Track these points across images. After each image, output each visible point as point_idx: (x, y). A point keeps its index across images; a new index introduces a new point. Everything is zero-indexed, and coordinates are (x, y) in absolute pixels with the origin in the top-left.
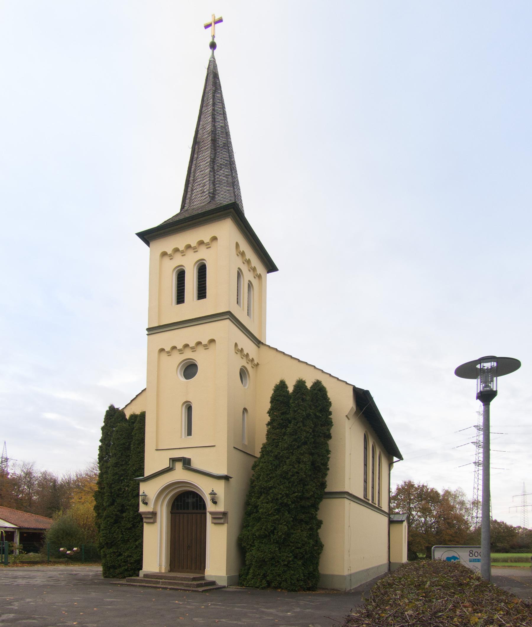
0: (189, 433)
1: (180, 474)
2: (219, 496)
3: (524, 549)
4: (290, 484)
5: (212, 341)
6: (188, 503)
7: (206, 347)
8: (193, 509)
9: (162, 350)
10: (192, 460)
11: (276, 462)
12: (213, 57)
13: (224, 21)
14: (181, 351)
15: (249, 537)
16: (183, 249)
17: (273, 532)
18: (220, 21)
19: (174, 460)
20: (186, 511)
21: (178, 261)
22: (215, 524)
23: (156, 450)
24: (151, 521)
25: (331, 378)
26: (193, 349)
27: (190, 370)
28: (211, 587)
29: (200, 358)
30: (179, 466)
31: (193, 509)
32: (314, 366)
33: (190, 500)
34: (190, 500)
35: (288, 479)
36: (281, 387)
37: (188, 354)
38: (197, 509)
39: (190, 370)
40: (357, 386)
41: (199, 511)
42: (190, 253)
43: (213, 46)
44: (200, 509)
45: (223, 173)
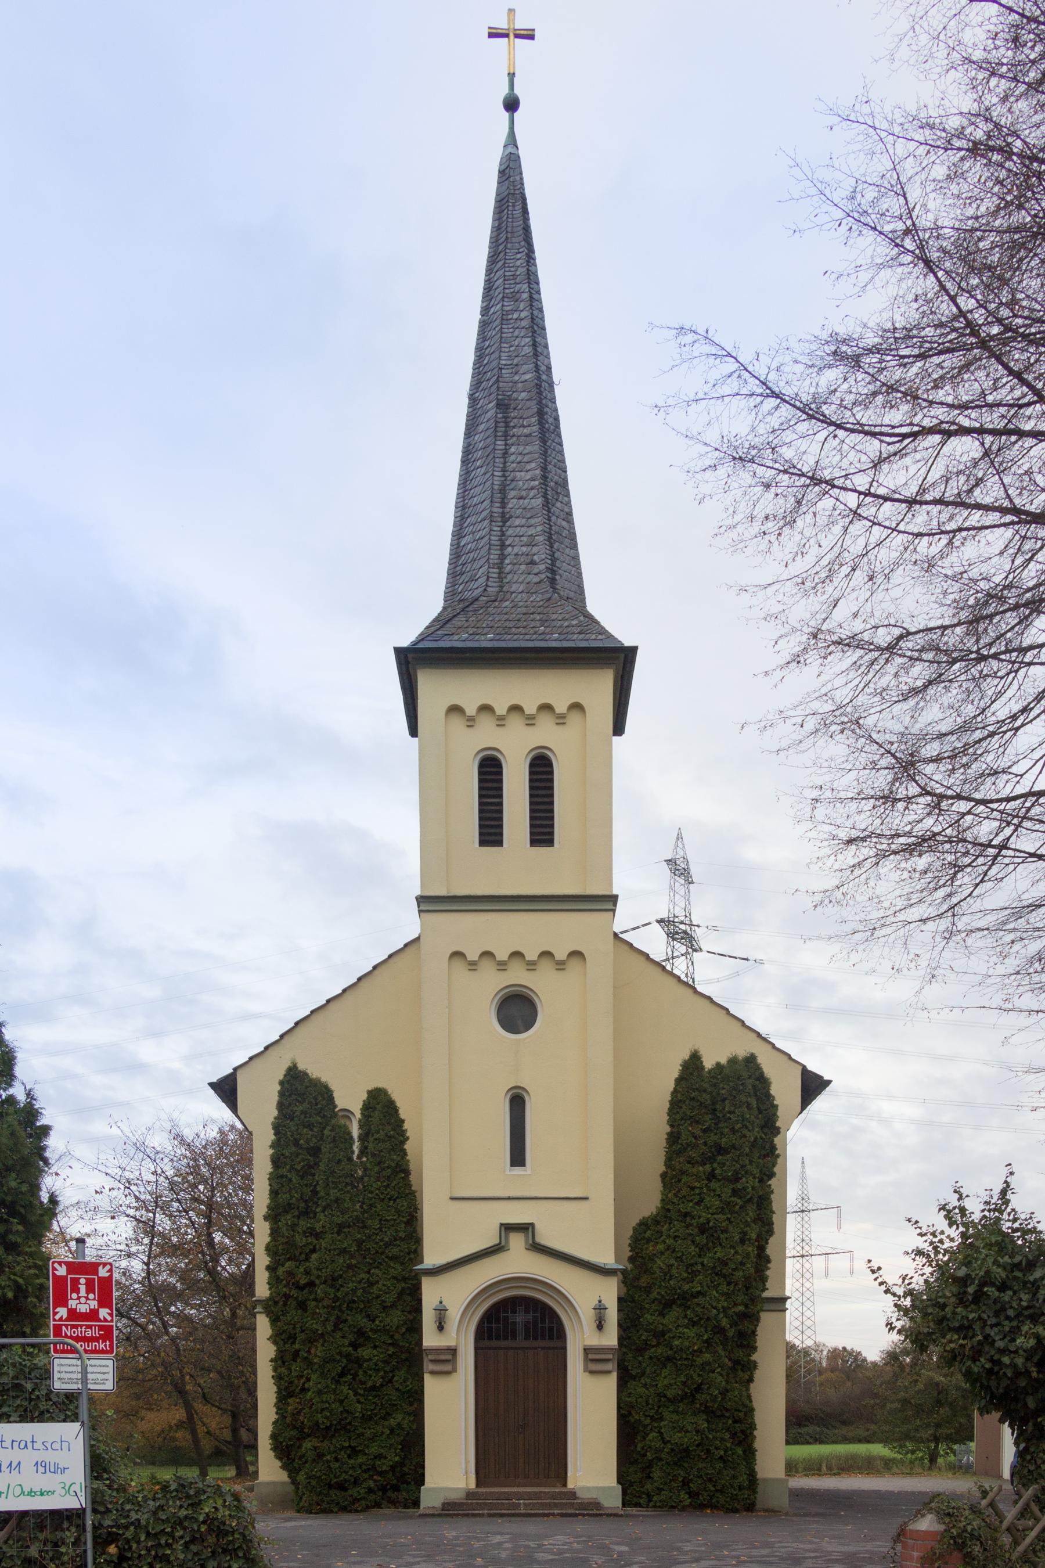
0: (518, 1158)
1: (518, 1262)
2: (591, 1309)
3: (811, 1429)
4: (732, 1287)
5: (577, 954)
6: (514, 1324)
7: (561, 965)
8: (527, 1338)
9: (457, 955)
10: (537, 1226)
11: (701, 1239)
12: (512, 140)
13: (536, 37)
14: (502, 966)
15: (651, 1401)
16: (504, 713)
17: (699, 1389)
18: (530, 36)
19: (508, 1228)
20: (510, 1343)
21: (487, 736)
22: (592, 1372)
23: (452, 1199)
24: (448, 1367)
25: (759, 1041)
26: (531, 966)
27: (517, 1010)
28: (590, 1510)
29: (544, 985)
30: (517, 1242)
31: (527, 1338)
32: (727, 1010)
33: (520, 1318)
34: (520, 1318)
35: (724, 1276)
36: (693, 1064)
37: (517, 976)
38: (535, 1338)
39: (517, 1010)
40: (810, 1068)
41: (551, 1344)
42: (516, 723)
43: (512, 105)
44: (551, 1338)
45: (525, 452)
